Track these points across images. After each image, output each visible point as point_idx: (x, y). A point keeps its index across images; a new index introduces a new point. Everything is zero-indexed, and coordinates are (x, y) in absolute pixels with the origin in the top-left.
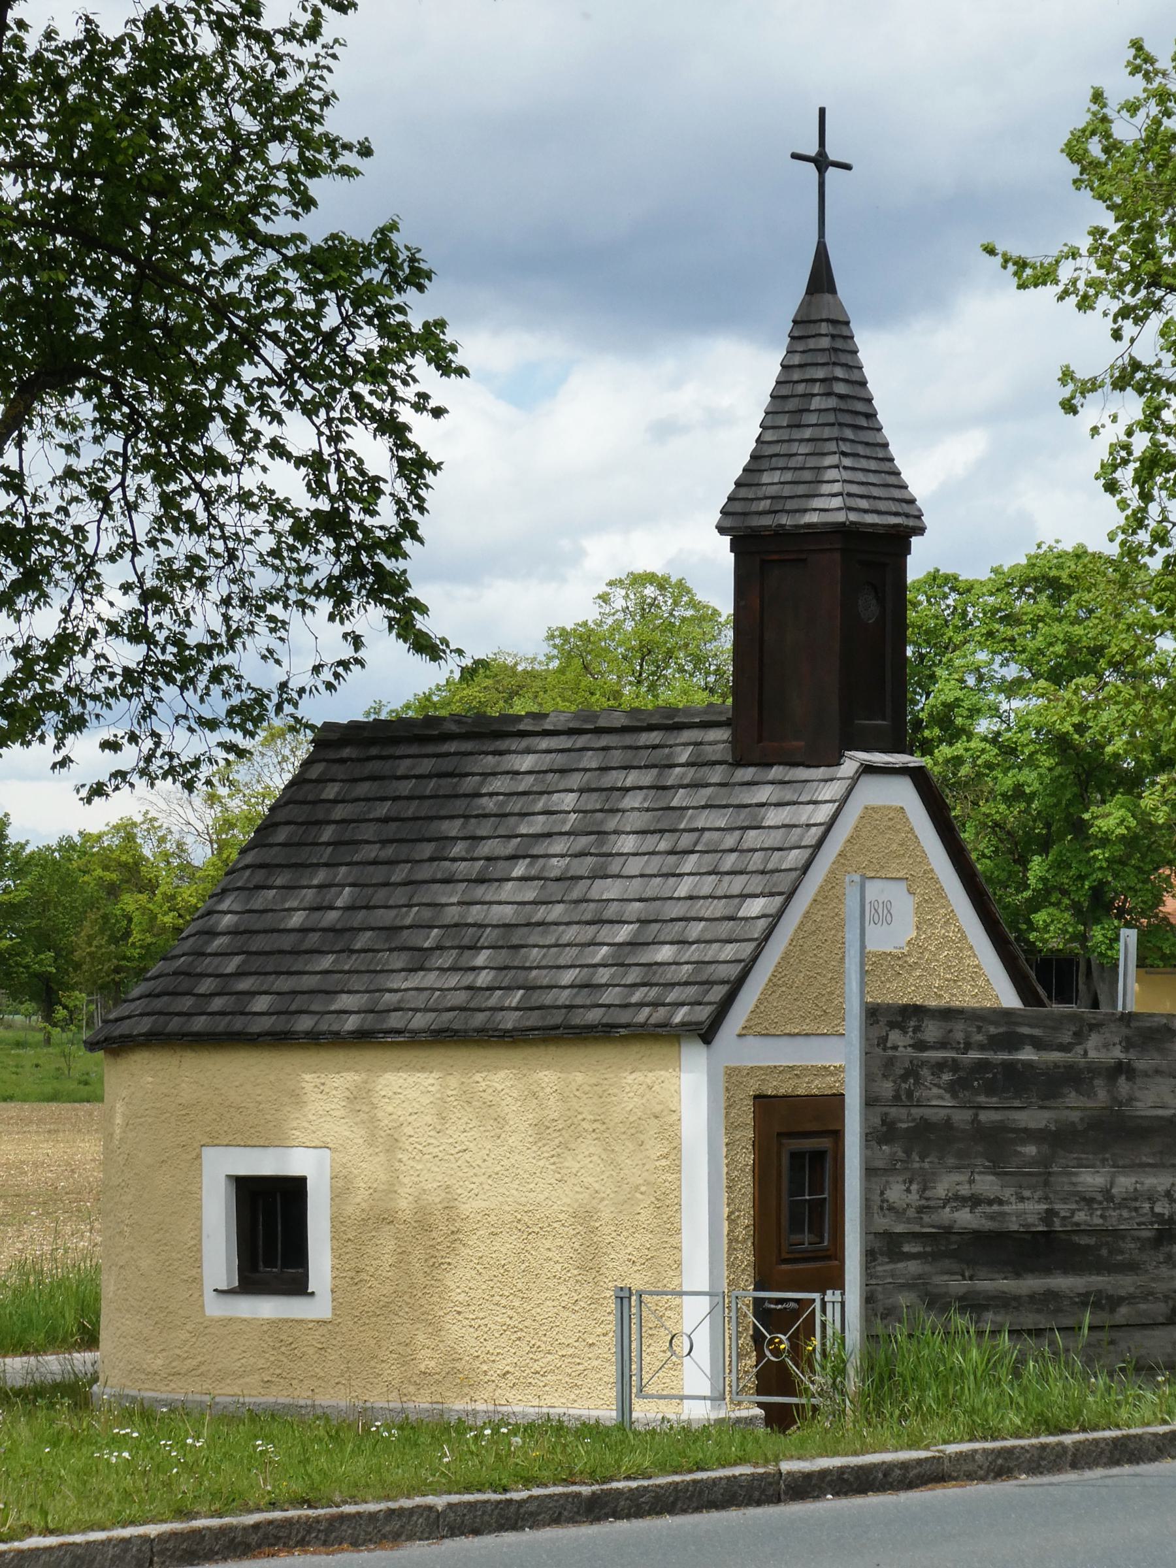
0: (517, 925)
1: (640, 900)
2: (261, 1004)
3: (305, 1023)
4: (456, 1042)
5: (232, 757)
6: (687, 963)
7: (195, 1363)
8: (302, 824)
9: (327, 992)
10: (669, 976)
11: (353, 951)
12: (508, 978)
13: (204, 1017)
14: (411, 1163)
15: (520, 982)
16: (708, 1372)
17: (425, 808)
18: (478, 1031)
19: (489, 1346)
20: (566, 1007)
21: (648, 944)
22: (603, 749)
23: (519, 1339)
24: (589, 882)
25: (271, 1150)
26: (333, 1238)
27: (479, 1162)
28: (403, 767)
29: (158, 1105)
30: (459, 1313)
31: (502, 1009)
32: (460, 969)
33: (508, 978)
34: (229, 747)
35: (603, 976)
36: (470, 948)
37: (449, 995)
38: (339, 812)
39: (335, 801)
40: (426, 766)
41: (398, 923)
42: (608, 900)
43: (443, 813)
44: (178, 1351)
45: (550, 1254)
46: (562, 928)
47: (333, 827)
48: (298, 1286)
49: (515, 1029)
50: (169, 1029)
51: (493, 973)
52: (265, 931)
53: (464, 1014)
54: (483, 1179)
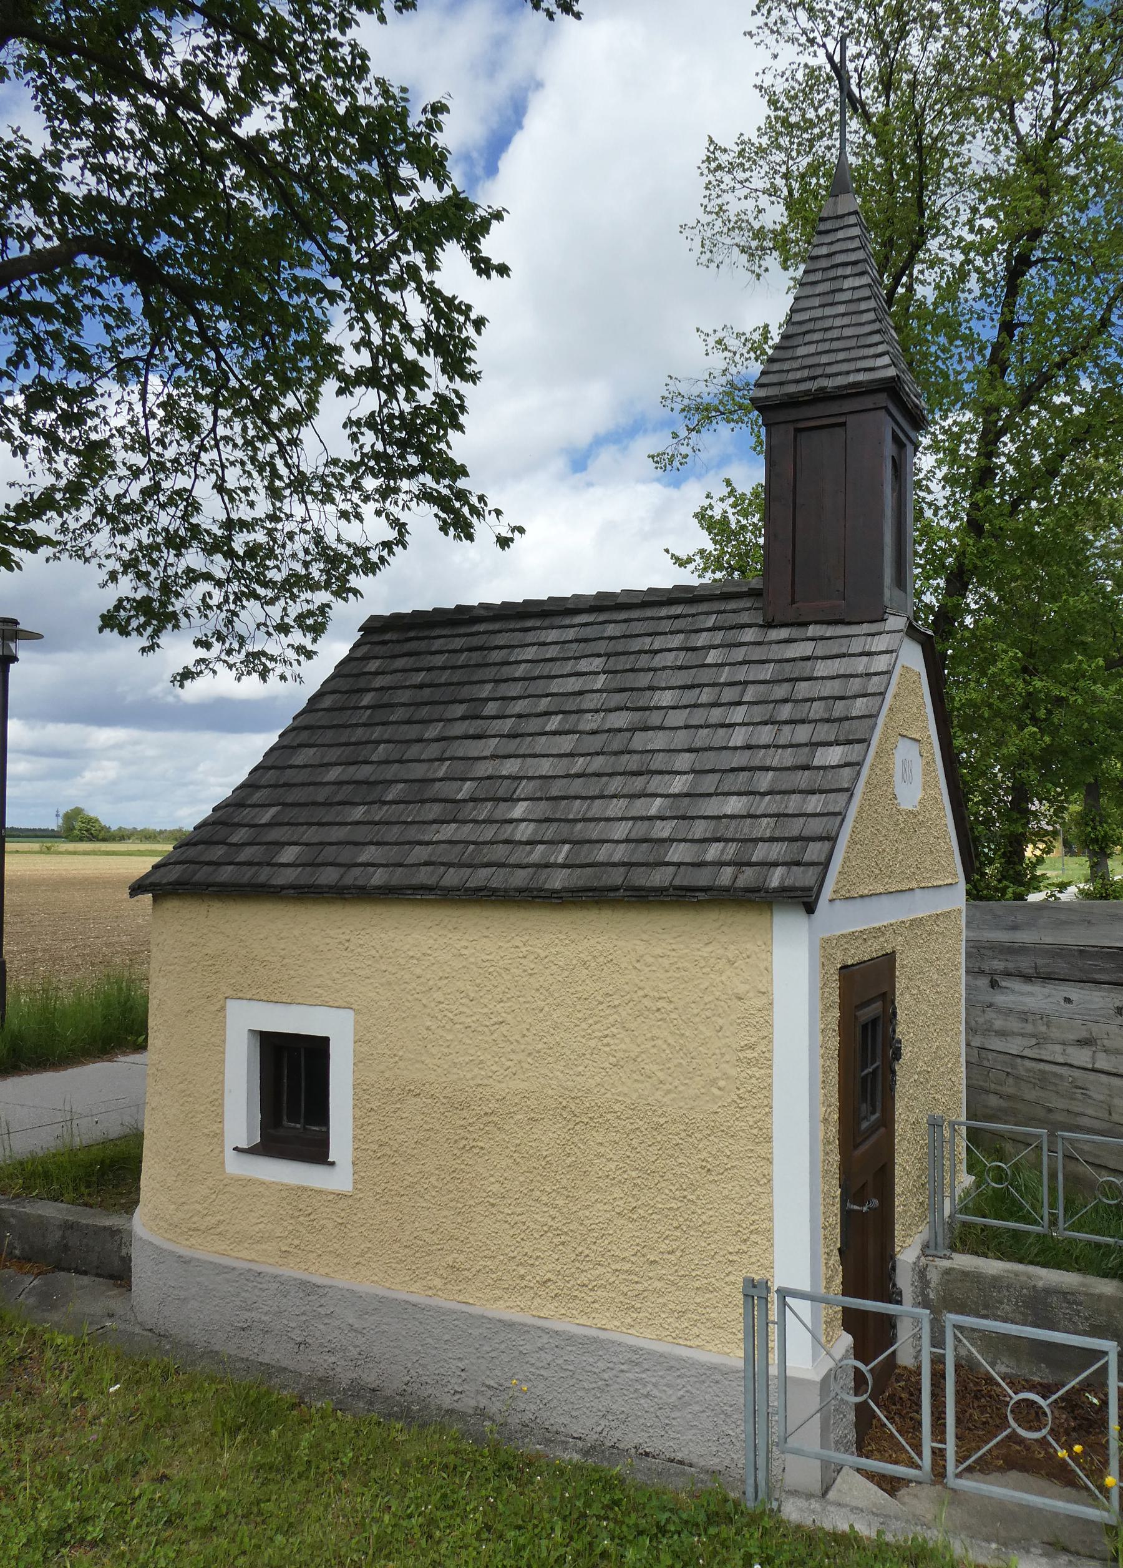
0: (555, 777)
1: (690, 750)
2: (289, 854)
3: (328, 876)
4: (492, 902)
5: (302, 658)
6: (765, 816)
7: (214, 1221)
8: (346, 692)
9: (356, 844)
10: (746, 830)
11: (385, 803)
12: (550, 831)
13: (231, 868)
14: (440, 1032)
15: (565, 835)
16: (808, 1321)
17: (458, 676)
18: (520, 890)
19: (527, 1247)
20: (624, 864)
21: (710, 795)
22: (625, 621)
23: (563, 1243)
24: (628, 734)
25: (294, 1007)
26: (355, 1106)
27: (518, 1037)
28: (437, 645)
29: (186, 954)
30: (493, 1205)
31: (547, 866)
32: (496, 822)
33: (550, 831)
34: (300, 650)
35: (663, 830)
36: (505, 800)
37: (485, 849)
38: (379, 682)
39: (376, 673)
40: (458, 643)
41: (430, 776)
42: (654, 751)
43: (475, 678)
44: (198, 1207)
45: (602, 1150)
46: (605, 779)
47: (373, 694)
48: (316, 1151)
49: (564, 890)
50: (196, 878)
51: (532, 826)
52: (303, 785)
53: (502, 871)
54: (521, 1056)
